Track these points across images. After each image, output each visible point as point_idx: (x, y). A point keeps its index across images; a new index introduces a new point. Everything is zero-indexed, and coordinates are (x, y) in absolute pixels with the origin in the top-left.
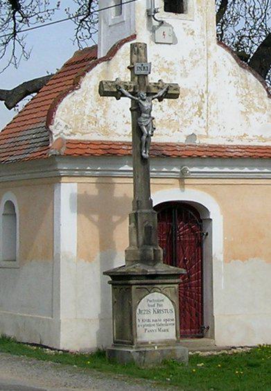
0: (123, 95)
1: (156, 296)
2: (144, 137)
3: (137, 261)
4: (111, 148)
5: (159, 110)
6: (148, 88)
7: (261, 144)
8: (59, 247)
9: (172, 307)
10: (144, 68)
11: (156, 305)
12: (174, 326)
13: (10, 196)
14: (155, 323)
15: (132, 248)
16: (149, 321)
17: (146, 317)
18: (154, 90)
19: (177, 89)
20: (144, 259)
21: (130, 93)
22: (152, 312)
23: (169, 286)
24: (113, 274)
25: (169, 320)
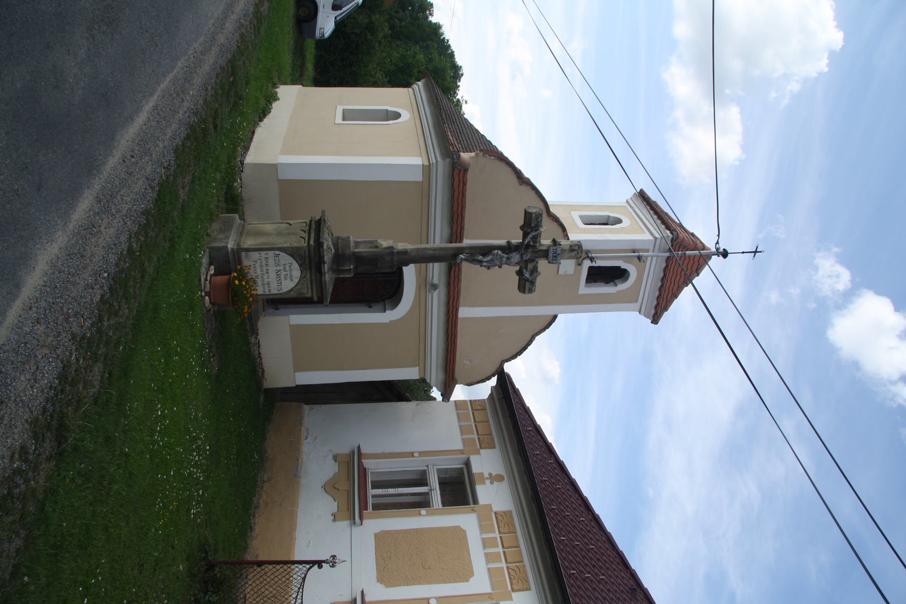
0: (525, 236)
1: (297, 273)
2: (480, 257)
3: (336, 248)
4: (458, 216)
5: (508, 274)
6: (532, 260)
7: (506, 407)
8: (502, 245)
9: (285, 290)
10: (556, 257)
11: (286, 273)
12: (262, 293)
13: (406, 115)
14: (265, 272)
15: (352, 244)
16: (267, 265)
17: (271, 262)
18: (530, 266)
19: (531, 291)
20: (339, 258)
21: (529, 242)
22: (278, 268)
23: (309, 286)
24: (322, 222)
25: (269, 287)
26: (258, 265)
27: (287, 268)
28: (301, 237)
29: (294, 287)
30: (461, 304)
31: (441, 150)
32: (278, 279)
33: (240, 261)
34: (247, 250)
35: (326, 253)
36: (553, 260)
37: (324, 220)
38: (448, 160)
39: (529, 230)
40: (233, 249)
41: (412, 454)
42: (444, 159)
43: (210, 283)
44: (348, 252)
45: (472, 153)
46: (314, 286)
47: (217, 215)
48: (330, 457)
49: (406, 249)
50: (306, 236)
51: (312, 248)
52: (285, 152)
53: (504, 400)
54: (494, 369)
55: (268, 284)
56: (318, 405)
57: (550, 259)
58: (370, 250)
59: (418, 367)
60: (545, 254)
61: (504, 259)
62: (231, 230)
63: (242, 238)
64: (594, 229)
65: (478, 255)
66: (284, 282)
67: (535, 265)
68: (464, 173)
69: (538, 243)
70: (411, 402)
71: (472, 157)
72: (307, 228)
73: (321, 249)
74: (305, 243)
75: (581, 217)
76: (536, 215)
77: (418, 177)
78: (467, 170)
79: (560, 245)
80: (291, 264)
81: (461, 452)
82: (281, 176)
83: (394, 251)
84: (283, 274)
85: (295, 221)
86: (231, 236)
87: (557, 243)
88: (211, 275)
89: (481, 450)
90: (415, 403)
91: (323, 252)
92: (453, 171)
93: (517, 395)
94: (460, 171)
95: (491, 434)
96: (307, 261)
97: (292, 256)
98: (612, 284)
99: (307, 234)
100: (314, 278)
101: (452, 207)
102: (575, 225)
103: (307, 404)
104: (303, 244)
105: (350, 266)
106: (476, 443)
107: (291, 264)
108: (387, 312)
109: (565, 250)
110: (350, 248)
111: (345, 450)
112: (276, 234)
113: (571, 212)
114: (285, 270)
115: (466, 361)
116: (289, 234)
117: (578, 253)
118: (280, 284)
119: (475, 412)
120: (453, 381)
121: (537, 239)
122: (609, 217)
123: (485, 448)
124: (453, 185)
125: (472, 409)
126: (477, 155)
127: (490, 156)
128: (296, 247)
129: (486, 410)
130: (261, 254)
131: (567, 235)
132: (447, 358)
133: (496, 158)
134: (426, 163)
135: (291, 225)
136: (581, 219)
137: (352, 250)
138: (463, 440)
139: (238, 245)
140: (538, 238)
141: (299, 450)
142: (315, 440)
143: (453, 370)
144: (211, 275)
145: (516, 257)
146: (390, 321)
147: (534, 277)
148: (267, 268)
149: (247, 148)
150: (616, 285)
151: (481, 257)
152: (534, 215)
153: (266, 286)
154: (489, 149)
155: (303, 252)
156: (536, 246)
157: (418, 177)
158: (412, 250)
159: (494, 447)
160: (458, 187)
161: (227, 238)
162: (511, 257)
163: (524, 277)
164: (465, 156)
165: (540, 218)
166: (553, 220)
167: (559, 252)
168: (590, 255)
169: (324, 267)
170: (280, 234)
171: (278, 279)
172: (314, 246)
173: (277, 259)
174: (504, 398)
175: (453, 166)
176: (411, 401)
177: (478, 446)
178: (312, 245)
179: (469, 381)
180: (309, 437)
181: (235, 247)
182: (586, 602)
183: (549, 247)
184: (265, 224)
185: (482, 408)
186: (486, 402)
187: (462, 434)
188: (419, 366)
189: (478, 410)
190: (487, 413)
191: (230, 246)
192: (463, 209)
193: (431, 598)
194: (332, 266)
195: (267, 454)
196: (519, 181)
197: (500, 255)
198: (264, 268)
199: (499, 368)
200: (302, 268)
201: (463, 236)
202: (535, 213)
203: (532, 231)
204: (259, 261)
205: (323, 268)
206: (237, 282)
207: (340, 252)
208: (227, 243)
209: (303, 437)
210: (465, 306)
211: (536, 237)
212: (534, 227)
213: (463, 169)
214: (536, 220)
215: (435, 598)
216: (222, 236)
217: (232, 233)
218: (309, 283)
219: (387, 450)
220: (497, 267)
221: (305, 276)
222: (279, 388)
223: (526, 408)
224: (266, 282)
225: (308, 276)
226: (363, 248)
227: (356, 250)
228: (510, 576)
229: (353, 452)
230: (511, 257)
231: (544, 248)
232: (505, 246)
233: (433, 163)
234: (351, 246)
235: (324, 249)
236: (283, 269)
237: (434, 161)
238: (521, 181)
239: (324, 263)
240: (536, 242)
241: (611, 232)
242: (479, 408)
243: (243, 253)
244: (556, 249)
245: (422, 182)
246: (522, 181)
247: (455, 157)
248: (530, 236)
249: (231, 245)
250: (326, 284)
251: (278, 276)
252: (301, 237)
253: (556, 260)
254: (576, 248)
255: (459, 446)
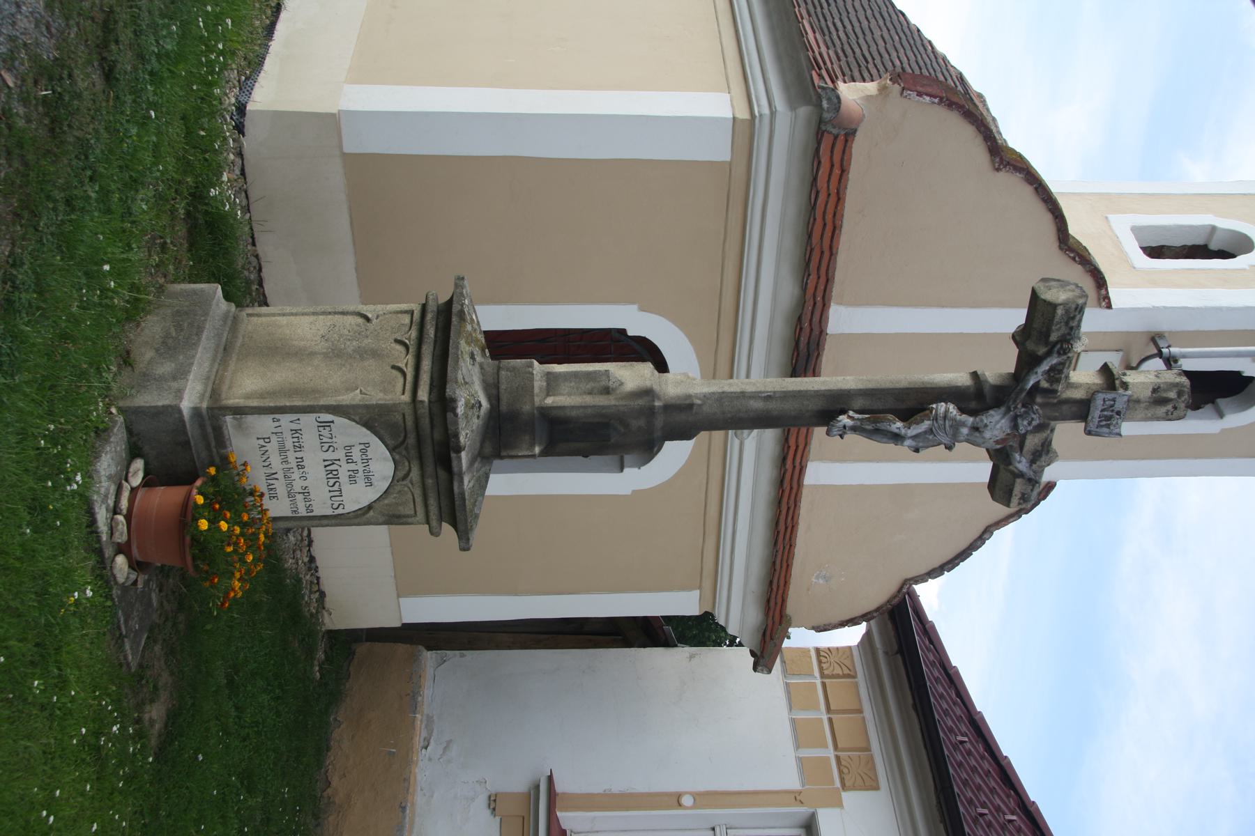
2: (898, 426)
3: (494, 397)
10: (1109, 418)
11: (352, 467)
14: (293, 464)
16: (299, 447)
17: (310, 438)
22: (330, 455)
23: (419, 500)
26: (273, 446)
27: (356, 454)
28: (394, 367)
29: (375, 501)
30: (811, 456)
31: (782, 72)
32: (333, 481)
33: (221, 440)
34: (239, 411)
35: (462, 423)
36: (1099, 426)
37: (461, 314)
38: (804, 111)
39: (1042, 350)
40: (196, 412)
41: (675, 800)
42: (792, 106)
43: (128, 517)
44: (527, 408)
45: (866, 84)
46: (432, 502)
47: (161, 289)
48: (482, 801)
49: (689, 396)
50: (406, 363)
51: (424, 411)
52: (362, 74)
53: (899, 657)
54: (878, 593)
55: (305, 492)
56: (457, 652)
57: (1092, 427)
58: (589, 400)
59: (699, 591)
60: (1081, 410)
61: (965, 431)
62: (195, 345)
63: (225, 370)
64: (1176, 271)
65: (890, 417)
66: (346, 488)
67: (1046, 439)
68: (846, 141)
69: (1063, 381)
70: (676, 649)
71: (869, 98)
72: (414, 333)
73: (450, 415)
74: (403, 394)
75: (1137, 231)
76: (1067, 311)
77: (721, 152)
78: (854, 132)
79: (1125, 386)
80: (367, 445)
81: (796, 797)
82: (351, 145)
83: (657, 404)
84: (344, 470)
85: (380, 308)
86: (194, 368)
87: (1117, 382)
88: (134, 491)
89: (844, 794)
90: (688, 650)
91: (456, 423)
92: (819, 143)
93: (931, 642)
94: (836, 138)
95: (867, 749)
96: (411, 440)
97: (368, 425)
98: (1208, 409)
99: (410, 358)
100: (430, 481)
101: (810, 236)
102: (1124, 257)
103: (429, 648)
104: (398, 395)
105: (532, 445)
106: (818, 704)
107: (367, 445)
108: (626, 470)
109: (1138, 401)
110: (532, 396)
111: (517, 783)
112: (326, 356)
113: (1110, 217)
114: (349, 460)
115: (817, 578)
116: (362, 354)
117: (1175, 408)
118: (337, 493)
119: (827, 681)
120: (780, 623)
121: (1060, 372)
122: (1213, 229)
123: (854, 788)
124: (815, 179)
125: (823, 675)
126: (883, 89)
127: (920, 94)
128: (378, 406)
129: (854, 677)
130: (278, 420)
131: (1107, 298)
132: (771, 583)
133: (936, 100)
134: (743, 114)
135: (368, 319)
136: (1135, 235)
137: (537, 400)
138: (801, 761)
139: (215, 394)
140: (1065, 370)
141: (407, 780)
142: (445, 749)
143: (784, 601)
144: (134, 491)
145: (997, 424)
146: (634, 491)
147: (1039, 467)
148: (299, 455)
149: (256, 64)
150: (1221, 415)
151: (899, 424)
152: (1060, 311)
153: (300, 497)
154: (917, 72)
155: (400, 418)
156: (1055, 391)
157: (721, 152)
158: (706, 397)
159: (876, 788)
160: (828, 181)
161: (181, 374)
162: (986, 426)
163: (1011, 467)
164: (852, 93)
165: (1077, 318)
166: (1074, 259)
167: (1119, 406)
168: (1165, 351)
169: (460, 459)
170: (335, 354)
171: (333, 481)
172: (430, 402)
173: (325, 432)
174: (900, 651)
175: (819, 128)
176: (676, 646)
177: (838, 784)
178: (422, 402)
179: (821, 621)
180: (432, 741)
181: (205, 405)
182: (982, 833)
183: (1093, 394)
184: (296, 314)
185: (846, 671)
186: (856, 653)
187: (798, 746)
188: (700, 588)
189: (838, 676)
190: (856, 685)
191: (186, 405)
192: (837, 232)
193: (686, 793)
194: (482, 447)
195: (329, 791)
196: (993, 162)
197: (954, 419)
198: (292, 456)
199: (894, 597)
200: (397, 457)
201: (830, 300)
202: (1064, 304)
203: (1049, 354)
204: (274, 439)
205: (455, 463)
206: (204, 524)
207: (504, 407)
208: (179, 393)
209: (418, 741)
210: (822, 459)
211: (1060, 367)
212: (1056, 343)
213: (843, 133)
214: (1067, 323)
215: (692, 794)
216: (166, 368)
217: (198, 355)
218: (418, 492)
219: (619, 784)
220: (943, 446)
221: (404, 478)
222: (362, 630)
223: (951, 672)
224: (297, 488)
225: (415, 474)
226: (570, 394)
227: (549, 401)
228: (842, 768)
229: (537, 787)
230: (986, 426)
231: (1078, 394)
232: (968, 387)
233: (761, 115)
234: (536, 390)
235: (456, 415)
236: (343, 459)
237: (766, 111)
238: (997, 160)
239: (459, 449)
240: (1058, 381)
241: (1226, 281)
242: (838, 671)
243: (229, 419)
244: (1114, 400)
245: (730, 163)
246: (1001, 159)
247: (825, 104)
248: (1045, 366)
249: (190, 398)
250: (463, 499)
251: (332, 475)
252: (394, 367)
253: (1108, 426)
254: (1172, 395)
255: (790, 780)
